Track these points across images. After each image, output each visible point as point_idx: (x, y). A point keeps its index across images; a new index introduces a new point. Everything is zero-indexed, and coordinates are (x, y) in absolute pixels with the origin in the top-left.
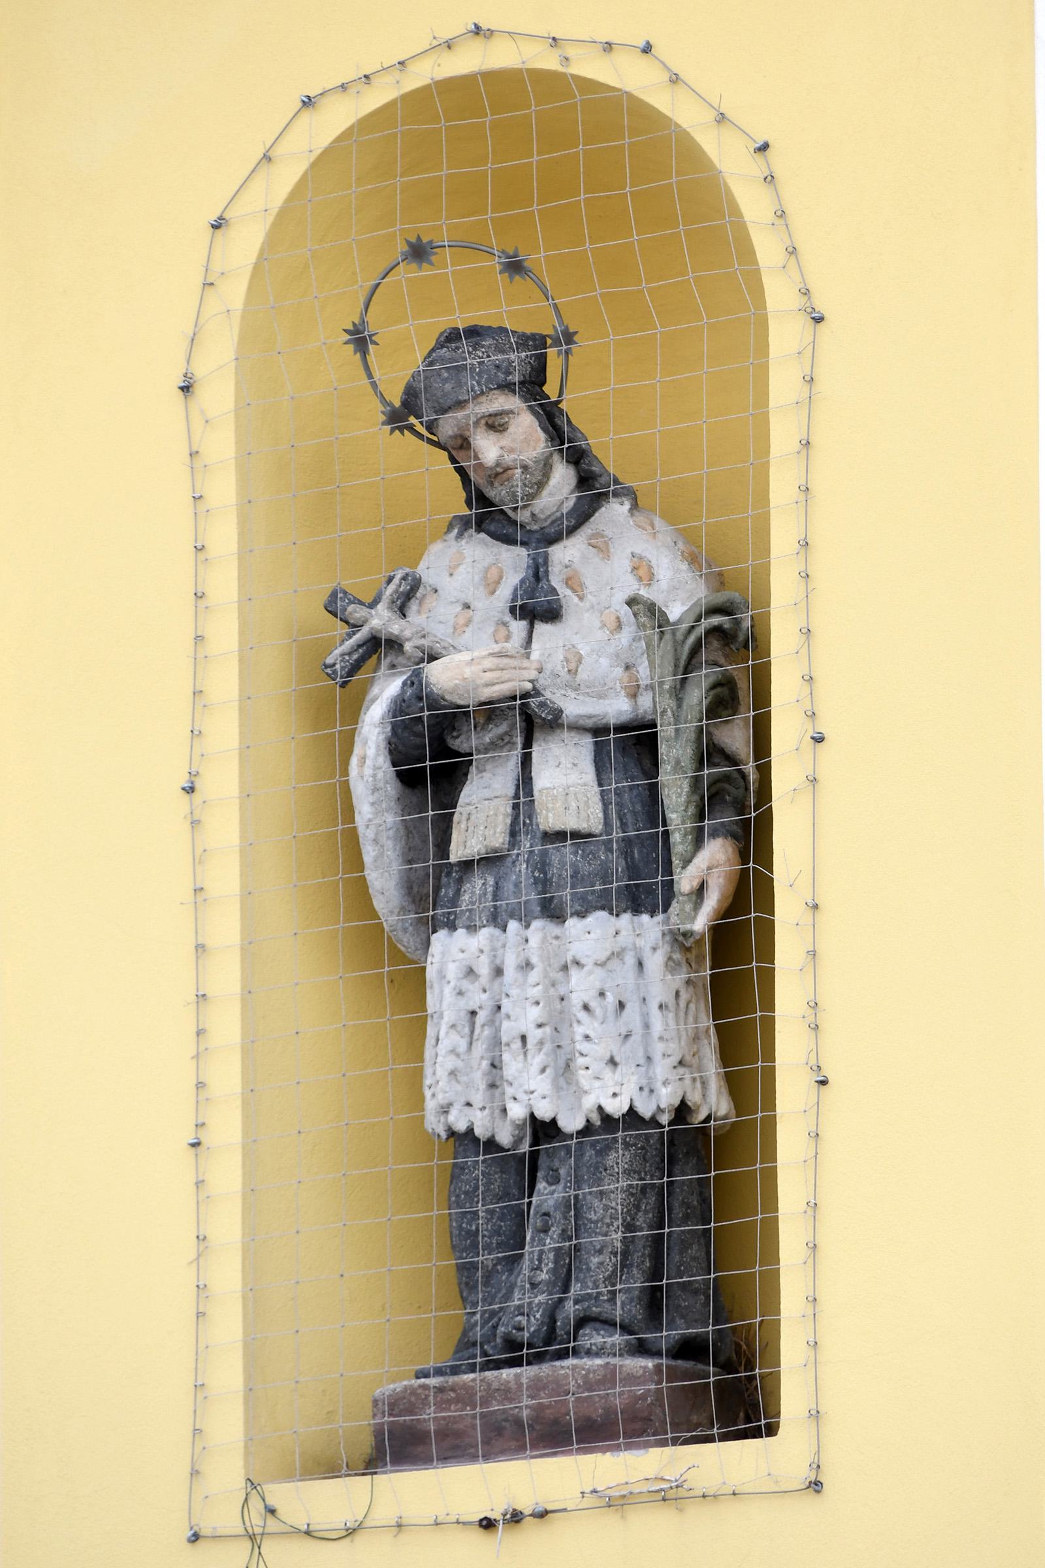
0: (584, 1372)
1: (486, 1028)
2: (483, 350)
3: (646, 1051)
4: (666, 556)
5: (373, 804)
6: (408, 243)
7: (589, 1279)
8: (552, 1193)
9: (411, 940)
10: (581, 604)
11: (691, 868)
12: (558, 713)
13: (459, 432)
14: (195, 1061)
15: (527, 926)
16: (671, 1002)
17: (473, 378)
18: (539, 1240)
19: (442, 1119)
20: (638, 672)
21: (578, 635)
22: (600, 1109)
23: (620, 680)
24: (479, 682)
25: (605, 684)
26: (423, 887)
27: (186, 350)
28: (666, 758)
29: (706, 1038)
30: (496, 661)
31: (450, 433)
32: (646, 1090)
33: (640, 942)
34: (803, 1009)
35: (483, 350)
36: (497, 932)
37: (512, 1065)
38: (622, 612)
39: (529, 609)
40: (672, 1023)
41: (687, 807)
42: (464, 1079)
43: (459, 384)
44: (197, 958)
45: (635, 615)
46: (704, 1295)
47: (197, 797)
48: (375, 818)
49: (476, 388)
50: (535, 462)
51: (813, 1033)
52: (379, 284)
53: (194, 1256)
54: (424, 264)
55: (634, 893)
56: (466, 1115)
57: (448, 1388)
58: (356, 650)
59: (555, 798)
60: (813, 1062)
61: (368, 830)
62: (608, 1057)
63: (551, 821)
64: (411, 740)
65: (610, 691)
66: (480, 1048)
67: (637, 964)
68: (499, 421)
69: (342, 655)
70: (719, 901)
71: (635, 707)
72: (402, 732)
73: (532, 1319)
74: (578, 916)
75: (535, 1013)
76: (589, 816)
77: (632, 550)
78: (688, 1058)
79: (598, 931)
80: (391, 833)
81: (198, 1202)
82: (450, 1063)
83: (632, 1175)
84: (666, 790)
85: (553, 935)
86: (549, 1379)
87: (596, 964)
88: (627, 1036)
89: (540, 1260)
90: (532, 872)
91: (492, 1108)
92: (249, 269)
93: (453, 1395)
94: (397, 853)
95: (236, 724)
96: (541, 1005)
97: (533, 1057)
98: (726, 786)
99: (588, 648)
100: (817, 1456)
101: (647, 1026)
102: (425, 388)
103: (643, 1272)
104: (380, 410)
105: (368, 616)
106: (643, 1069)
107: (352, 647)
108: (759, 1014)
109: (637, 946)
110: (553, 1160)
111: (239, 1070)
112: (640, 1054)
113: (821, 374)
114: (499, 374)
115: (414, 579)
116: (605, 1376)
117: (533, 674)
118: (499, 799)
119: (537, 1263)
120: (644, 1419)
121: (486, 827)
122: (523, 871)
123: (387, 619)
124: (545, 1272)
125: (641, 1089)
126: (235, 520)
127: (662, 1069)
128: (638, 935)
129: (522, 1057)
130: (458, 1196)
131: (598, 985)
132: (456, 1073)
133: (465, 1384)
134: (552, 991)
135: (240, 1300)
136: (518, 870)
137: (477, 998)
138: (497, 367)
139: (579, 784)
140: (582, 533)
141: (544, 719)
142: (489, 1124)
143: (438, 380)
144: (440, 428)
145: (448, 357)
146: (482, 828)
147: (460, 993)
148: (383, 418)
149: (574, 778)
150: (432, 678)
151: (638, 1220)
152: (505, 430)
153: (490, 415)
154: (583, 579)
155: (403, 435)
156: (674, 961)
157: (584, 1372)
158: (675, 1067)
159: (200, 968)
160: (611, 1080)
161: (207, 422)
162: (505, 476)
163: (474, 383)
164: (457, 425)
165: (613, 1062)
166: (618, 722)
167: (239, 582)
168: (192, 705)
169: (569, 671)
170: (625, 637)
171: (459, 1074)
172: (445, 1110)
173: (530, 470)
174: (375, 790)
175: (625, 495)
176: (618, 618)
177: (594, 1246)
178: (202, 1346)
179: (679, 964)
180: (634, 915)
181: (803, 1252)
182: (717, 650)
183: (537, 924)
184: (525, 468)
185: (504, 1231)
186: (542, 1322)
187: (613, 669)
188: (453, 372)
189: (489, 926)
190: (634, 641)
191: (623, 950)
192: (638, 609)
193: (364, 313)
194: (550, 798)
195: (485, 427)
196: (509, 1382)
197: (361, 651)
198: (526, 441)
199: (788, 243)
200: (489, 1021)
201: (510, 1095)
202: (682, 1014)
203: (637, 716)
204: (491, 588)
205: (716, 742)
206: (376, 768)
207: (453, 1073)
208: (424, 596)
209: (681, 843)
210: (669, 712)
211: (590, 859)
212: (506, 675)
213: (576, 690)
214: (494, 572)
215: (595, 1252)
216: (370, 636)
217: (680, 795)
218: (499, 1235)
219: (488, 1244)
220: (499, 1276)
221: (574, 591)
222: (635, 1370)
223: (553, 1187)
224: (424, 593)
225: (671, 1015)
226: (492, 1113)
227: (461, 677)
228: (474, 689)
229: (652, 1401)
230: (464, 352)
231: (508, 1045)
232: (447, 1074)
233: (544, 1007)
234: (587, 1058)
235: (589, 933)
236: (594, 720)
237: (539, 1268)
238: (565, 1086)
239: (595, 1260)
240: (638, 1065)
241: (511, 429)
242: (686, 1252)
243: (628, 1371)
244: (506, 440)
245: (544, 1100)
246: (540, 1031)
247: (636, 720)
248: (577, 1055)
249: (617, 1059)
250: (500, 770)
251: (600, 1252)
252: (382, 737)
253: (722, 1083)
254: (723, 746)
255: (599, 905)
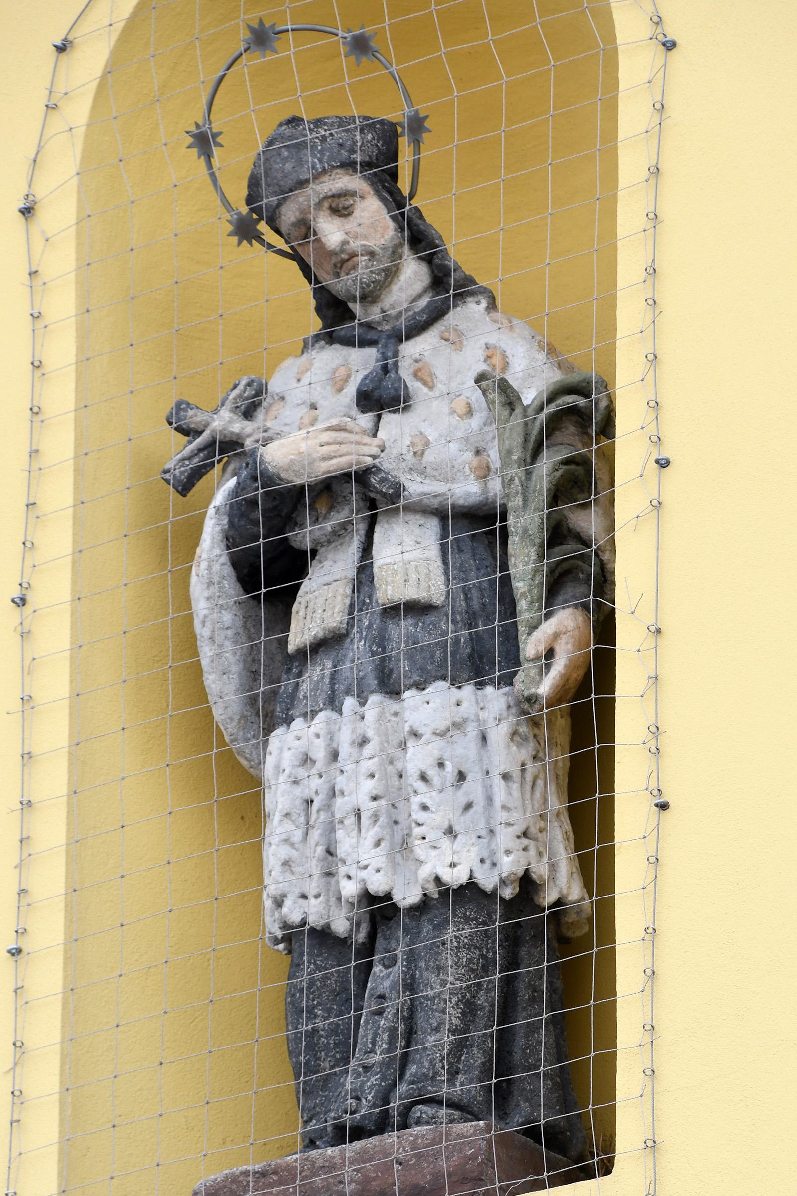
0: (412, 1138)
1: (322, 813)
2: (326, 127)
3: (488, 822)
4: (521, 346)
5: (208, 599)
6: (251, 29)
7: (425, 1059)
8: (388, 976)
9: (254, 753)
10: (431, 393)
11: (538, 634)
12: (398, 490)
13: (301, 217)
14: (18, 870)
15: (363, 704)
16: (516, 774)
17: (314, 156)
18: (373, 1023)
19: (277, 915)
20: (489, 456)
21: (426, 422)
22: (438, 880)
23: (470, 464)
24: (315, 456)
25: (453, 467)
26: (270, 704)
27: (28, 174)
28: (513, 530)
29: (556, 821)
30: (333, 434)
31: (293, 219)
32: (488, 862)
33: (483, 715)
34: (643, 734)
35: (326, 127)
36: (334, 715)
37: (345, 842)
38: (473, 398)
39: (375, 398)
40: (516, 793)
41: (534, 576)
42: (297, 869)
43: (300, 163)
44: (24, 766)
45: (484, 392)
46: (551, 1080)
47: (28, 609)
48: (210, 614)
49: (318, 166)
50: (382, 249)
51: (654, 758)
52: (225, 74)
53: (12, 1066)
54: (268, 52)
55: (478, 666)
56: (301, 907)
57: (270, 1172)
58: (196, 455)
59: (395, 572)
60: (653, 785)
61: (205, 629)
62: (446, 825)
63: (389, 592)
64: (248, 529)
65: (459, 474)
66: (315, 835)
67: (480, 736)
68: (343, 202)
69: (184, 459)
70: (566, 666)
71: (485, 490)
72: (239, 521)
73: (364, 1101)
74: (418, 688)
75: (369, 787)
76: (430, 587)
77: (486, 341)
78: (533, 830)
79: (438, 700)
80: (230, 633)
81: (16, 1009)
82: (285, 852)
83: (472, 950)
84: (513, 559)
85: (392, 711)
86: (376, 1149)
87: (434, 733)
88: (468, 806)
89: (374, 1043)
90: (369, 646)
91: (327, 895)
92: (94, 85)
93: (275, 1177)
94: (237, 657)
95: (70, 532)
96: (376, 777)
97: (368, 830)
98: (580, 563)
99: (436, 434)
100: (652, 1185)
101: (489, 800)
102: (265, 172)
103: (485, 1051)
104: (196, 119)
105: (209, 419)
106: (485, 841)
107: (192, 451)
108: (597, 746)
109: (481, 718)
110: (389, 943)
111: (63, 874)
112: (482, 824)
113: (674, 102)
114: (343, 152)
115: (260, 385)
116: (434, 1138)
117: (375, 450)
118: (338, 582)
119: (370, 1046)
120: (475, 1179)
121: (324, 611)
122: (361, 648)
123: (228, 419)
124: (378, 1053)
125: (482, 861)
126: (74, 334)
127: (505, 838)
128: (481, 709)
129: (355, 832)
130: (293, 995)
131: (436, 754)
132: (291, 863)
133: (288, 1165)
134: (390, 768)
135: (57, 1104)
136: (355, 647)
137: (314, 785)
138: (341, 145)
139: (421, 559)
140: (435, 330)
141: (385, 494)
142: (324, 912)
143: (279, 161)
144: (283, 217)
145: (288, 134)
146: (320, 612)
147: (296, 782)
148: (230, 228)
149: (415, 554)
150: (267, 457)
151: (479, 999)
152: (350, 214)
153: (333, 196)
154: (434, 370)
155: (251, 245)
156: (520, 735)
157: (412, 1138)
158: (518, 837)
159: (26, 778)
160: (448, 848)
161: (47, 240)
162: (350, 263)
163: (316, 160)
164: (299, 209)
165: (450, 832)
166: (466, 504)
167: (76, 394)
168: (24, 521)
169: (415, 453)
170: (475, 422)
171: (293, 865)
172: (279, 903)
173: (377, 257)
174: (210, 583)
175: (481, 293)
176: (468, 404)
177: (431, 1024)
178: (15, 1153)
179: (525, 739)
180: (479, 689)
181: (640, 979)
182: (574, 435)
183: (374, 699)
184: (372, 254)
185: (342, 1030)
186: (374, 1104)
187: (462, 453)
188: (294, 151)
189: (325, 709)
190: (485, 425)
191: (465, 720)
192: (487, 385)
193: (207, 115)
194: (390, 572)
195: (329, 212)
196: (334, 1157)
197: (201, 455)
198: (373, 226)
199: (658, 98)
200: (324, 806)
201: (344, 874)
202: (528, 788)
203: (487, 498)
204: (338, 386)
205: (571, 526)
206: (210, 561)
207: (286, 863)
208: (271, 405)
209: (527, 610)
210: (517, 481)
211: (431, 630)
212: (344, 448)
213: (422, 474)
214: (342, 371)
215: (432, 1030)
216: (211, 439)
217: (527, 564)
218: (337, 1034)
219: (325, 1045)
220: (337, 1078)
221: (425, 383)
222: (465, 1129)
223: (390, 970)
224: (272, 402)
225: (515, 786)
226: (328, 901)
227: (297, 453)
228: (309, 464)
229: (482, 1159)
230: (305, 129)
231: (341, 822)
232: (280, 863)
233: (380, 779)
234: (423, 827)
235: (428, 703)
236: (440, 499)
237: (372, 1051)
238: (401, 862)
239: (431, 1039)
240: (479, 837)
241: (357, 213)
242: (533, 1036)
243: (459, 1131)
244: (350, 224)
245: (378, 874)
246: (375, 804)
247: (485, 505)
248: (413, 825)
249: (456, 828)
250: (340, 556)
251: (437, 1029)
252: (218, 528)
253: (574, 870)
254: (578, 530)
255: (439, 674)
